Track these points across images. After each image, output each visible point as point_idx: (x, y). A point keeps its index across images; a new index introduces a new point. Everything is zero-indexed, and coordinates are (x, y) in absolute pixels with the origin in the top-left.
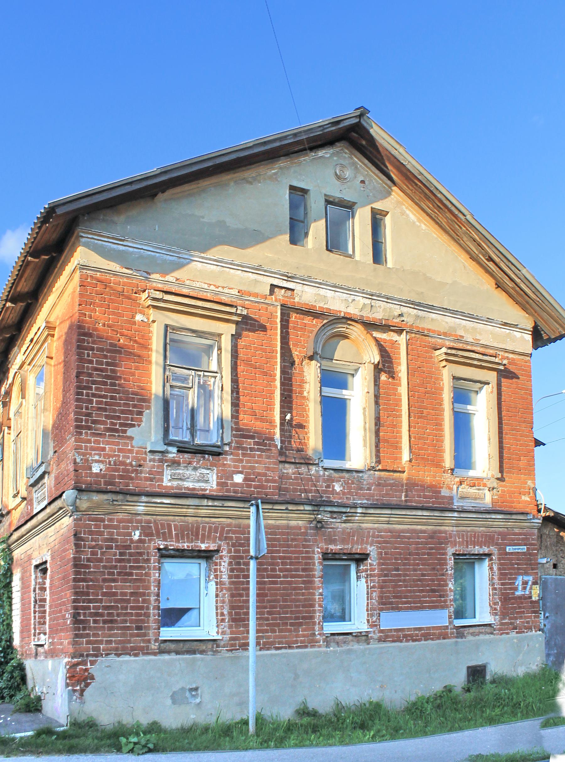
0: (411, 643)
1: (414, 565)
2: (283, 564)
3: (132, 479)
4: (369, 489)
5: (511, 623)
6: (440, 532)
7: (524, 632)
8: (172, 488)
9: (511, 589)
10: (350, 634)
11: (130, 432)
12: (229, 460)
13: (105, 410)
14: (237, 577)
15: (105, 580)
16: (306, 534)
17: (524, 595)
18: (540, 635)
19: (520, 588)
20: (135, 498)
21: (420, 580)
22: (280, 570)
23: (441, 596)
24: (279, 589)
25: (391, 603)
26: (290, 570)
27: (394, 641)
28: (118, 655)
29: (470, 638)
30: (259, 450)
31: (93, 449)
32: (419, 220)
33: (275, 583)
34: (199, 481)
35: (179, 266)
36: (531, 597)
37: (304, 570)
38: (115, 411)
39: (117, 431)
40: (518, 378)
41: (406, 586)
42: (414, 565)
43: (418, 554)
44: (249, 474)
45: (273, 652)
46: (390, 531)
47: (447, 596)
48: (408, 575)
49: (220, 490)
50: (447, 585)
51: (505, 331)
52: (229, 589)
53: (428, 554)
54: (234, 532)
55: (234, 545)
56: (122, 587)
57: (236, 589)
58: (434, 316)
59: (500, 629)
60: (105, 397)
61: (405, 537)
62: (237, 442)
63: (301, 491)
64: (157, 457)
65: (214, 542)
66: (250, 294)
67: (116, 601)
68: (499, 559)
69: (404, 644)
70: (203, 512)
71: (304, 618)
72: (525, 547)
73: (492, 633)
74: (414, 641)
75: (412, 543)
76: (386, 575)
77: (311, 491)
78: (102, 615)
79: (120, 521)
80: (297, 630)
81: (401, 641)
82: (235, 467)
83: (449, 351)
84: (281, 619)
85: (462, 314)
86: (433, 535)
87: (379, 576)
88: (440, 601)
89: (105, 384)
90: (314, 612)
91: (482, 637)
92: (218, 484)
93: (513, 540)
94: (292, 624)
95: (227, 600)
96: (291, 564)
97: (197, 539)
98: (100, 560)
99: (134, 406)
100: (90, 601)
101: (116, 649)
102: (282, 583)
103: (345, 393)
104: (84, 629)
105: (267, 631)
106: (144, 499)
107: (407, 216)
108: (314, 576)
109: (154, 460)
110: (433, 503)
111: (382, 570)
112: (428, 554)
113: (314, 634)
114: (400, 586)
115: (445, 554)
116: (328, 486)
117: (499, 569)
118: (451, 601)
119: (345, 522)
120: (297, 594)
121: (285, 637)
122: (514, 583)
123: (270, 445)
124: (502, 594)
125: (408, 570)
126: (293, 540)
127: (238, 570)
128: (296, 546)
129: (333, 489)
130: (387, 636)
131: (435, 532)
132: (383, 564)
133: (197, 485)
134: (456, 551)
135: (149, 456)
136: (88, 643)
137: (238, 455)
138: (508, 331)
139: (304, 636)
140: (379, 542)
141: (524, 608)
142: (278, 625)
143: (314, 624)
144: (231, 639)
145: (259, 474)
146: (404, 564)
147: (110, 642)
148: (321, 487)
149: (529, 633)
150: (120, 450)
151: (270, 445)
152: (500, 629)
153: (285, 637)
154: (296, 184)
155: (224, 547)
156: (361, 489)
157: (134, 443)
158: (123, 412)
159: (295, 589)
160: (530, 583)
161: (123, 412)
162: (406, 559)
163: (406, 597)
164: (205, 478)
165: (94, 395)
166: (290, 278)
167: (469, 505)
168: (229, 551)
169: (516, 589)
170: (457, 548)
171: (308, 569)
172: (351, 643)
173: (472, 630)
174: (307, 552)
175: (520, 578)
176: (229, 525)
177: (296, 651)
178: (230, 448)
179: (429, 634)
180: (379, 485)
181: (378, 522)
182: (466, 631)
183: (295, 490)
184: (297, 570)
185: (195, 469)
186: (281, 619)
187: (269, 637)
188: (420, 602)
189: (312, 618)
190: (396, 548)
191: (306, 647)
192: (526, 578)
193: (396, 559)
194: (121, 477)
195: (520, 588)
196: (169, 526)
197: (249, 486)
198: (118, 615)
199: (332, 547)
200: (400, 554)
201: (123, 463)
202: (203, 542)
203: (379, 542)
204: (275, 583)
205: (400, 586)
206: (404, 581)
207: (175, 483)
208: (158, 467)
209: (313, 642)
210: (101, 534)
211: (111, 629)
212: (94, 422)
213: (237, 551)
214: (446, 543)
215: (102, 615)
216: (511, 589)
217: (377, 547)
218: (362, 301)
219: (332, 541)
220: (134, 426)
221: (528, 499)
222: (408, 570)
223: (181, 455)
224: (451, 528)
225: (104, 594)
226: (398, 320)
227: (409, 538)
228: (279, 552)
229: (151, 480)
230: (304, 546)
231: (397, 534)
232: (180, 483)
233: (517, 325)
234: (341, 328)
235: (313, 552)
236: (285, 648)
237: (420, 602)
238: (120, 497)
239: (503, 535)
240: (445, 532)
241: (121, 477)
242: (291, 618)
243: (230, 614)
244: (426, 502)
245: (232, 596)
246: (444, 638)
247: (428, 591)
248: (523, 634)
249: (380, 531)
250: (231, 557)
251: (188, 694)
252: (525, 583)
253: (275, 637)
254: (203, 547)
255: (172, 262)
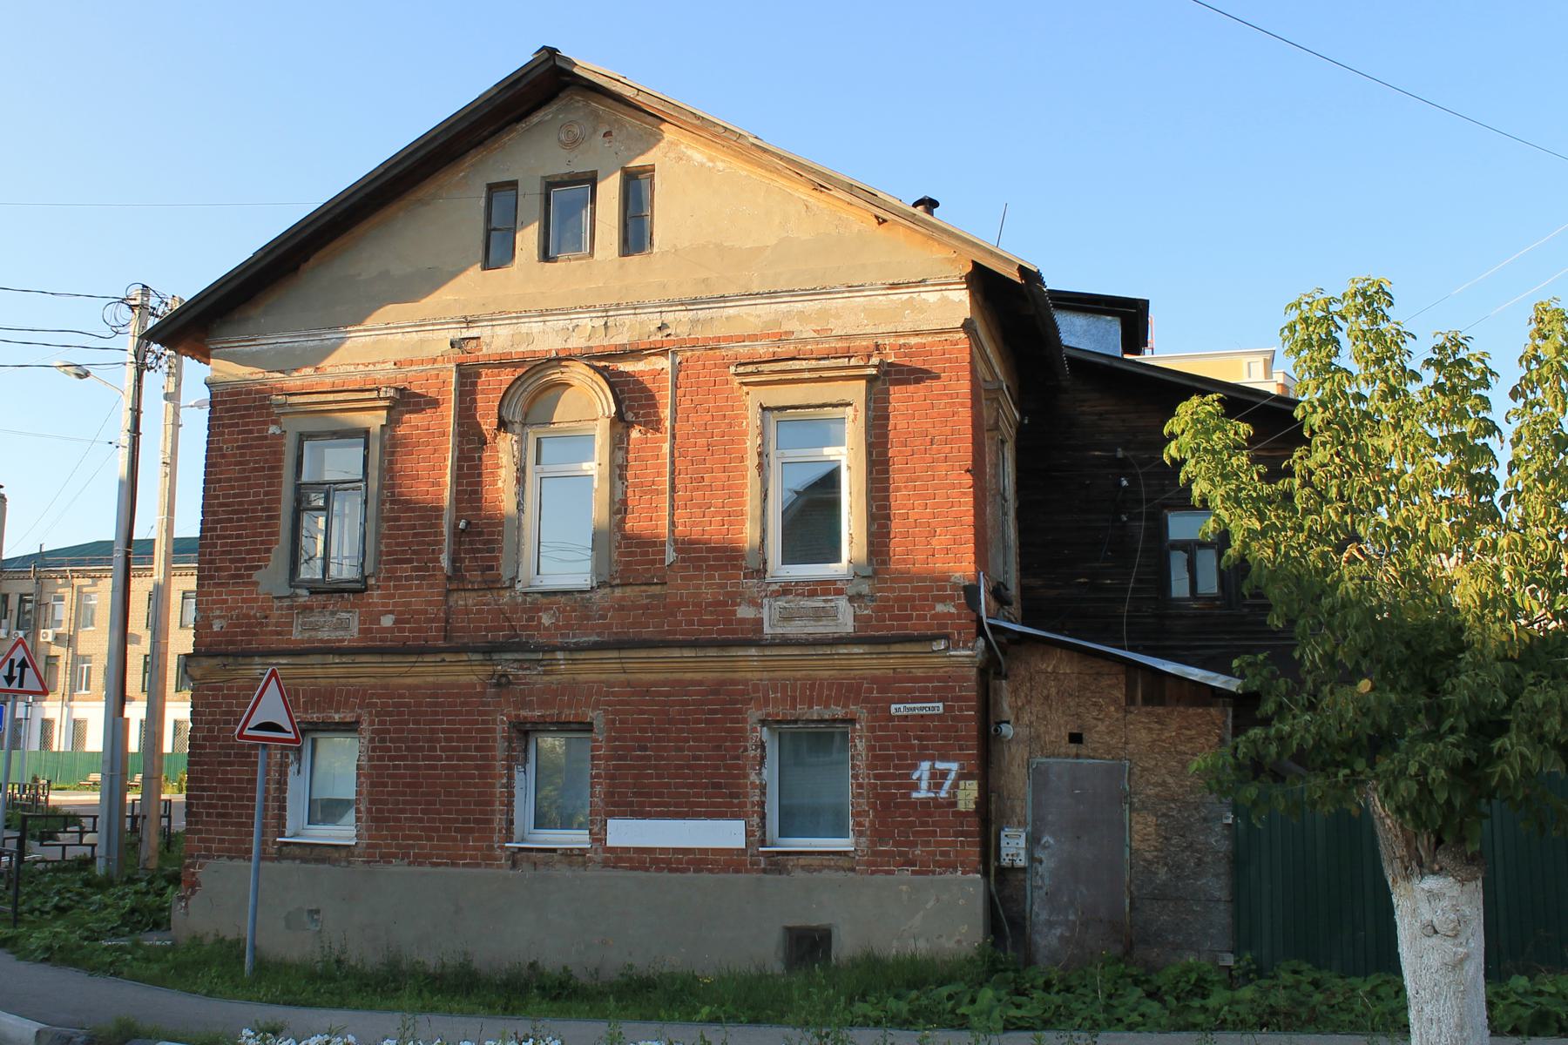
0: (665, 874)
1: (677, 740)
2: (448, 740)
3: (255, 634)
4: (603, 617)
5: (901, 854)
6: (734, 682)
7: (933, 872)
8: (302, 641)
9: (899, 786)
10: (554, 850)
11: (256, 576)
12: (375, 596)
13: (229, 553)
14: (380, 758)
15: (221, 763)
16: (483, 694)
17: (935, 799)
18: (973, 881)
19: (924, 785)
20: (248, 660)
21: (689, 767)
22: (443, 749)
23: (732, 795)
24: (439, 777)
25: (631, 804)
26: (457, 749)
27: (632, 869)
28: (231, 858)
29: (799, 874)
30: (418, 577)
31: (215, 602)
32: (711, 160)
33: (434, 767)
34: (336, 629)
35: (327, 352)
36: (955, 804)
37: (478, 749)
38: (240, 552)
39: (241, 577)
40: (938, 377)
41: (659, 776)
42: (677, 740)
43: (683, 722)
44: (401, 613)
45: (427, 869)
46: (629, 684)
47: (746, 795)
48: (662, 758)
49: (359, 640)
50: (746, 776)
51: (902, 296)
52: (369, 776)
53: (707, 721)
54: (379, 696)
55: (378, 714)
56: (238, 772)
57: (378, 776)
58: (731, 311)
59: (870, 864)
60: (230, 537)
61: (660, 694)
62: (387, 571)
63: (488, 629)
64: (286, 603)
65: (352, 710)
66: (412, 363)
67: (231, 790)
68: (872, 729)
69: (653, 874)
70: (335, 671)
71: (476, 821)
72: (941, 705)
73: (853, 870)
74: (671, 870)
75: (674, 703)
76: (620, 758)
77: (502, 629)
78: (215, 807)
79: (239, 689)
80: (466, 840)
81: (647, 870)
82: (384, 605)
83: (741, 370)
84: (442, 821)
85: (791, 292)
86: (717, 688)
87: (608, 758)
88: (732, 805)
89: (231, 520)
90: (493, 812)
91: (826, 874)
92: (360, 631)
93: (912, 690)
94: (457, 830)
95: (365, 791)
96: (459, 740)
97: (330, 707)
98: (217, 739)
99: (262, 543)
100: (204, 789)
101: (229, 850)
102: (444, 767)
103: (1503, 349)
104: (197, 823)
105: (419, 838)
106: (257, 660)
107: (689, 159)
108: (494, 758)
109: (281, 608)
110: (719, 632)
111: (616, 749)
112: (707, 721)
113: (491, 848)
114: (650, 776)
115: (745, 721)
116: (531, 619)
117: (871, 748)
118: (753, 805)
119: (546, 673)
120: (467, 785)
121: (447, 848)
122: (909, 776)
123: (434, 568)
124: (877, 796)
125: (665, 749)
126: (463, 704)
127: (381, 749)
128: (468, 713)
129: (540, 623)
130: (620, 860)
131: (722, 683)
132: (616, 739)
133: (334, 635)
134: (768, 715)
135: (277, 604)
136: (200, 840)
137: (387, 588)
138: (906, 297)
139: (475, 848)
140: (609, 704)
141: (935, 824)
142: (437, 830)
143: (492, 830)
144: (369, 846)
145: (417, 612)
146: (658, 740)
147: (222, 841)
148: (520, 620)
149: (948, 876)
150: (244, 601)
151: (434, 568)
152: (870, 864)
153: (447, 848)
154: (495, 179)
155: (365, 718)
156: (588, 618)
157: (260, 590)
158: (249, 552)
159: (462, 777)
160: (952, 775)
161: (249, 552)
162: (660, 731)
163: (660, 795)
164: (344, 626)
165: (218, 537)
166: (468, 322)
167: (794, 631)
168: (372, 723)
169: (916, 787)
170: (770, 709)
171: (485, 748)
172: (558, 866)
173: (803, 861)
174: (484, 722)
175: (925, 765)
176: (373, 687)
177: (462, 870)
178: (378, 580)
179: (706, 861)
180: (622, 608)
181: (603, 671)
182: (792, 860)
183: (478, 629)
184: (467, 749)
185: (333, 613)
186: (442, 821)
187: (422, 847)
188: (688, 804)
189: (490, 821)
190: (642, 712)
191: (478, 865)
192: (940, 765)
193: (643, 730)
194: (243, 634)
195: (924, 785)
196: (297, 692)
197: (402, 630)
198: (233, 807)
199: (523, 713)
200: (650, 721)
201: (247, 616)
202: (337, 711)
203: (609, 704)
204: (434, 767)
205: (650, 776)
206: (656, 767)
207: (307, 635)
208: (286, 616)
209: (489, 858)
210: (219, 705)
211: (224, 824)
212: (218, 569)
213: (382, 722)
214: (747, 702)
215: (215, 807)
216: (899, 786)
217: (606, 711)
218: (587, 322)
219: (524, 704)
220: (259, 567)
221: (953, 610)
222: (665, 749)
223: (314, 598)
224: (757, 675)
225: (219, 781)
226: (659, 337)
227: (668, 694)
228: (441, 722)
229: (278, 633)
230: (481, 713)
231: (645, 690)
232: (313, 633)
233: (924, 281)
234: (555, 375)
235: (494, 722)
236: (446, 864)
237: (688, 804)
238: (231, 660)
239: (884, 684)
240: (745, 682)
241: (243, 634)
242: (456, 821)
243: (369, 811)
244: (705, 632)
245: (373, 785)
246: (737, 871)
247: (706, 786)
248: (930, 877)
249: (611, 685)
250: (373, 732)
251: (305, 917)
252: (938, 778)
253: (433, 848)
254: (337, 718)
255: (313, 349)
